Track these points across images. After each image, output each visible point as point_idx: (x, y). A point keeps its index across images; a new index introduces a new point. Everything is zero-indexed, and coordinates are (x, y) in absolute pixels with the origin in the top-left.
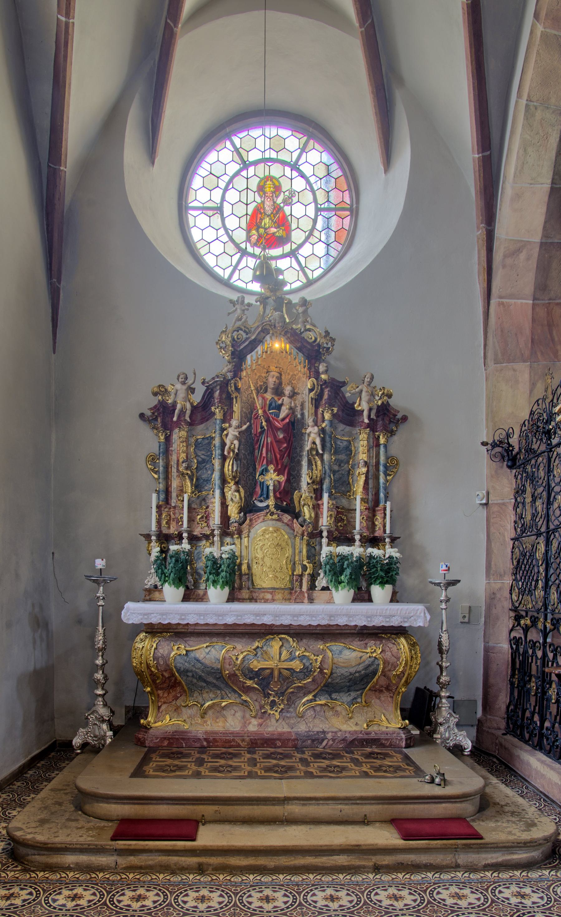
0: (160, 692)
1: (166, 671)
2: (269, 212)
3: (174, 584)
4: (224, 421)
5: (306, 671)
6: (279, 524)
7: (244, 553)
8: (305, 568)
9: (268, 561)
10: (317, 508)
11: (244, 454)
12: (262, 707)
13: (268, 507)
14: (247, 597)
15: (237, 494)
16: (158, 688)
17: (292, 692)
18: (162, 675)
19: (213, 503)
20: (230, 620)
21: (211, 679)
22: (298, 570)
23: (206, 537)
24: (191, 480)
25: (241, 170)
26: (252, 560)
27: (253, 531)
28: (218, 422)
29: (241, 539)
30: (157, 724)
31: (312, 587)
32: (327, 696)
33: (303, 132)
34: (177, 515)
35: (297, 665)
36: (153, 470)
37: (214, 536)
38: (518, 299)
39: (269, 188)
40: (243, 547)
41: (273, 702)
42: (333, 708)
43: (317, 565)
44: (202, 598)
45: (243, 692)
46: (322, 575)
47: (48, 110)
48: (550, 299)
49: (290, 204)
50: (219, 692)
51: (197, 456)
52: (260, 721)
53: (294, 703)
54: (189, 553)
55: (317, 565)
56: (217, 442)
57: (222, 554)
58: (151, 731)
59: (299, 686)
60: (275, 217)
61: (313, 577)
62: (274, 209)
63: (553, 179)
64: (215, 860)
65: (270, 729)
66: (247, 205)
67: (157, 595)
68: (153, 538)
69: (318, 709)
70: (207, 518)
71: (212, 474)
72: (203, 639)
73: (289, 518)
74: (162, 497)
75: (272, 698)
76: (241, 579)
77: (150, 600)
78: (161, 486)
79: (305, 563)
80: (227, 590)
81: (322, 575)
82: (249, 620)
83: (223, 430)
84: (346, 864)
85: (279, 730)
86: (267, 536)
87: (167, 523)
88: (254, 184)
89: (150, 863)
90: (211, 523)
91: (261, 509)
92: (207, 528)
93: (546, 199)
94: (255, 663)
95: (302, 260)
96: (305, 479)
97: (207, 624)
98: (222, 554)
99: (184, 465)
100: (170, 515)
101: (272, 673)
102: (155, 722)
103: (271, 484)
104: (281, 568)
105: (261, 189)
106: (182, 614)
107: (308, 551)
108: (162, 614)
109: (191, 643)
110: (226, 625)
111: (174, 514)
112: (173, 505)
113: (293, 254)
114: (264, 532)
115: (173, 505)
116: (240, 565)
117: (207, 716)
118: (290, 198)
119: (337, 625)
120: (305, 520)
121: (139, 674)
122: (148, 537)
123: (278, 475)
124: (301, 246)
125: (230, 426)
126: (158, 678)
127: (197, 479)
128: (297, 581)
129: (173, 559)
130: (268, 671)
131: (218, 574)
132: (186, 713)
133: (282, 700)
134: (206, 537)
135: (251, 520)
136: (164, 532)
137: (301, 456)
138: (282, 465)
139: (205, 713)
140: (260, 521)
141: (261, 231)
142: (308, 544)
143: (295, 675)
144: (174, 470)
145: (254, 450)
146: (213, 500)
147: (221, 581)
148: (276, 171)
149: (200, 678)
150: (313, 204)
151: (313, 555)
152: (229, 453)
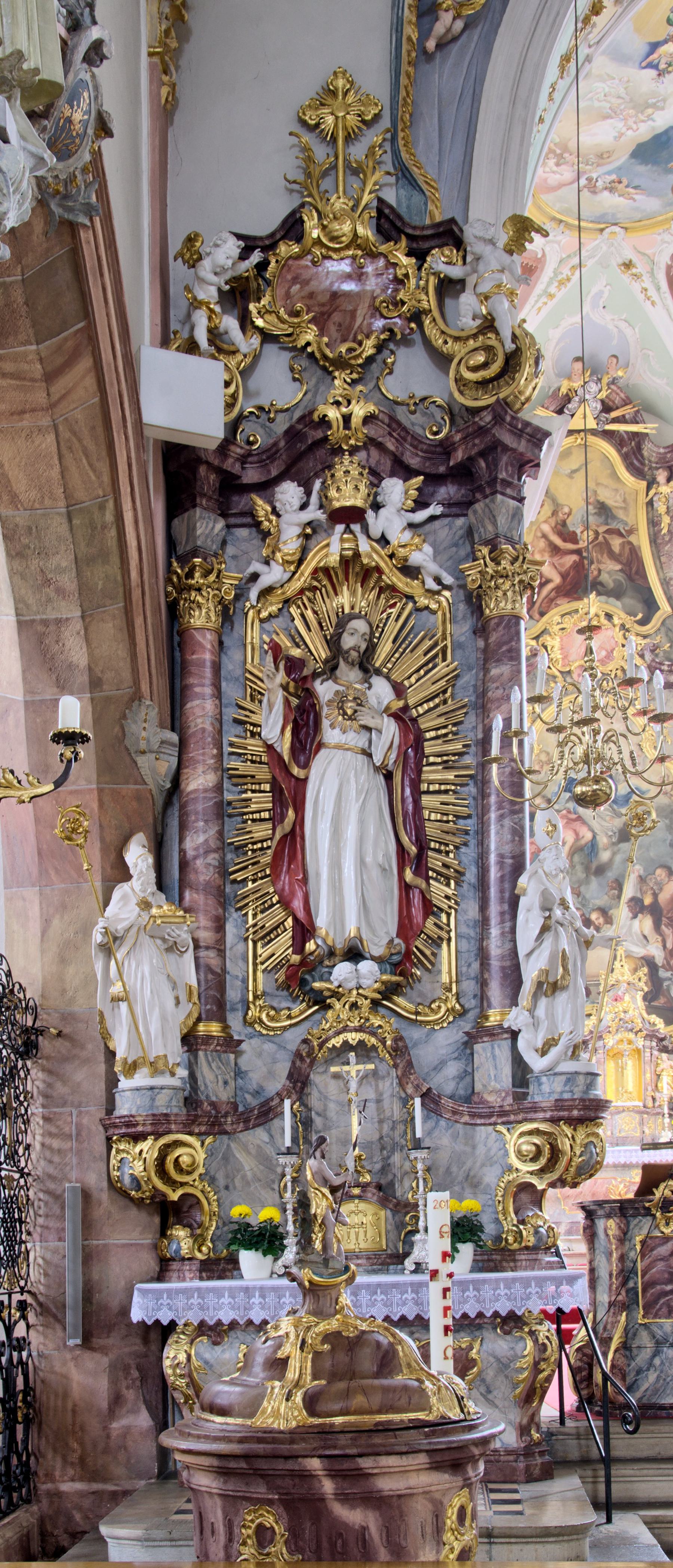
63: (16, 609)
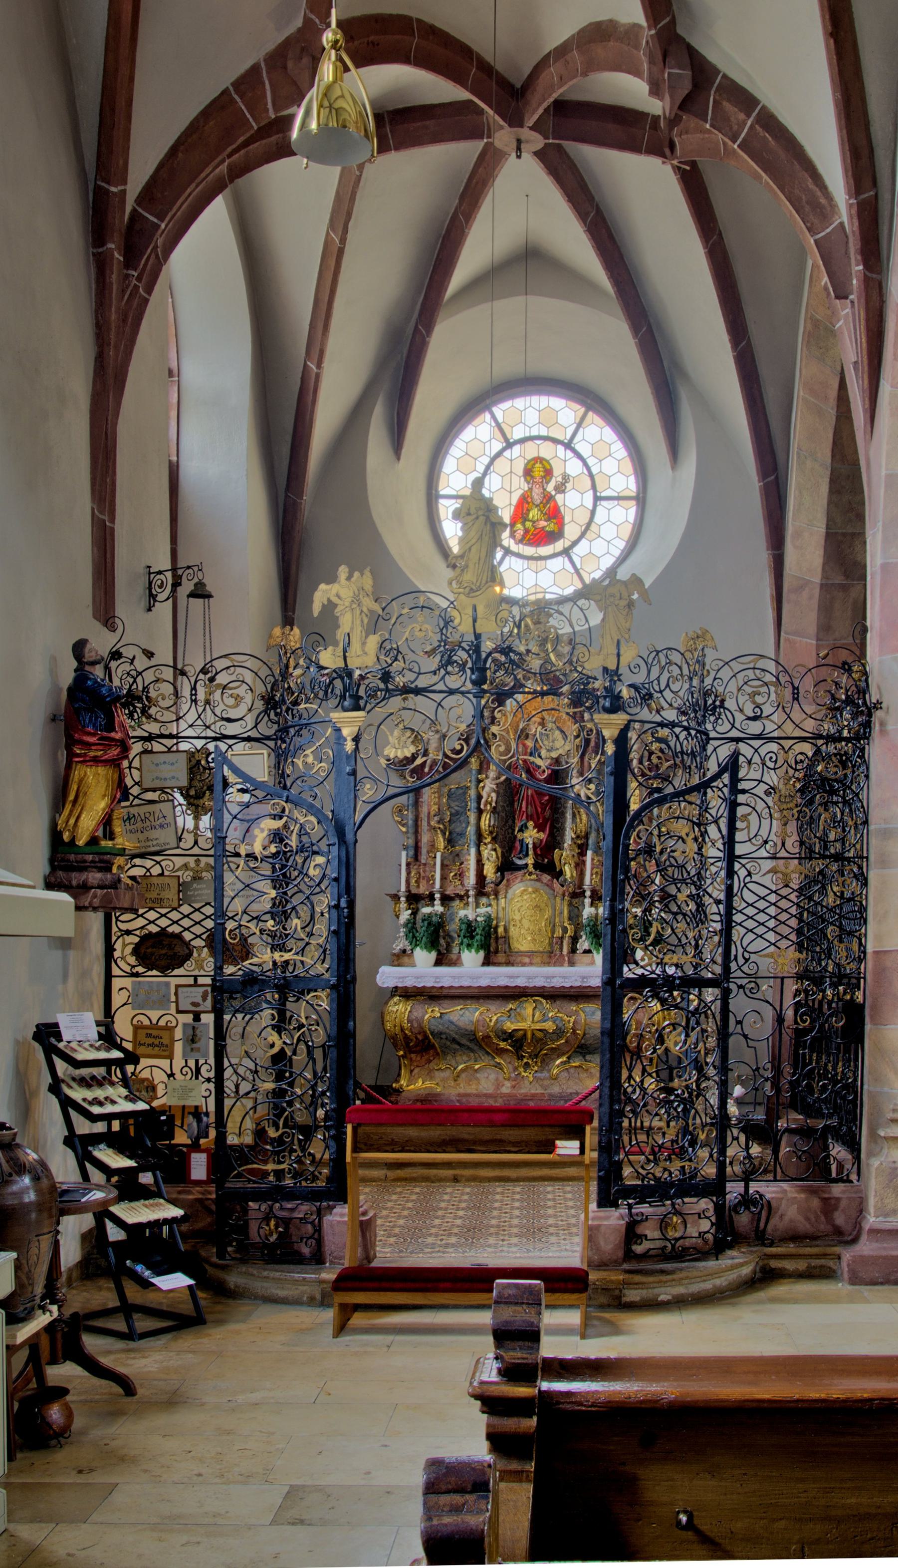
0: (413, 1056)
1: (419, 1033)
2: (539, 501)
3: (426, 948)
4: (480, 772)
5: (559, 1032)
6: (538, 884)
7: (501, 915)
8: (565, 930)
9: (526, 923)
10: (580, 866)
11: (503, 806)
12: (516, 1069)
13: (526, 865)
14: (503, 961)
15: (494, 853)
16: (411, 1052)
17: (546, 1054)
18: (416, 1038)
19: (467, 860)
20: (484, 983)
21: (464, 1041)
22: (559, 932)
23: (461, 898)
24: (444, 834)
25: (504, 450)
26: (509, 922)
27: (510, 892)
28: (474, 772)
29: (498, 900)
30: (410, 1088)
31: (573, 950)
32: (581, 1058)
33: (582, 403)
34: (427, 874)
35: (550, 1026)
36: (400, 823)
37: (468, 897)
38: (803, 637)
39: (538, 472)
40: (500, 909)
41: (527, 1064)
42: (587, 1070)
43: (578, 927)
44: (456, 962)
45: (496, 1054)
46: (584, 937)
47: (289, 438)
48: (835, 640)
49: (563, 492)
50: (472, 1054)
51: (450, 807)
52: (514, 1083)
53: (547, 1064)
54: (442, 916)
55: (578, 927)
56: (472, 793)
57: (477, 916)
58: (404, 1094)
59: (553, 1048)
60: (544, 507)
61: (575, 939)
62: (544, 497)
63: (827, 525)
64: (468, 1172)
65: (523, 1091)
66: (511, 492)
67: (406, 959)
68: (403, 899)
69: (572, 1071)
70: (461, 875)
71: (467, 827)
72: (457, 1002)
73: (549, 877)
74: (412, 853)
75: (525, 1060)
76: (497, 942)
77: (399, 965)
78: (411, 842)
79: (566, 924)
80: (482, 953)
81: (584, 937)
82: (503, 982)
83: (479, 781)
84: (576, 1175)
85: (533, 1091)
86: (525, 897)
87: (416, 882)
88: (519, 468)
89: (415, 1175)
90: (466, 882)
91: (519, 868)
92: (460, 887)
93: (823, 542)
94: (508, 1024)
95: (577, 560)
96: (569, 835)
97: (461, 987)
98: (477, 916)
99: (436, 818)
100: (419, 873)
101: (525, 1035)
102: (408, 1086)
103: (529, 841)
104: (540, 930)
105: (528, 472)
106: (437, 977)
107: (570, 912)
108: (417, 978)
109: (445, 1006)
110: (480, 987)
111: (424, 871)
112: (423, 861)
113: (566, 552)
114: (523, 892)
115: (423, 861)
116: (497, 927)
117: (460, 1080)
118: (563, 484)
119: (589, 987)
120: (566, 880)
121: (394, 1038)
122: (396, 897)
123: (538, 832)
124: (575, 543)
125: (487, 777)
126: (412, 1040)
127: (450, 833)
128: (557, 943)
129: (426, 923)
130: (521, 1032)
131: (472, 937)
132: (439, 1075)
133: (536, 1062)
134: (461, 898)
135: (508, 880)
136: (413, 892)
137: (565, 808)
138: (544, 818)
139: (458, 1076)
140: (517, 881)
141: (528, 524)
142: (570, 904)
143: (548, 1036)
144: (424, 823)
145: (513, 801)
146: (468, 857)
147: (475, 944)
148: (546, 451)
149: (454, 1040)
150: (591, 492)
151: (575, 916)
152: (485, 805)
